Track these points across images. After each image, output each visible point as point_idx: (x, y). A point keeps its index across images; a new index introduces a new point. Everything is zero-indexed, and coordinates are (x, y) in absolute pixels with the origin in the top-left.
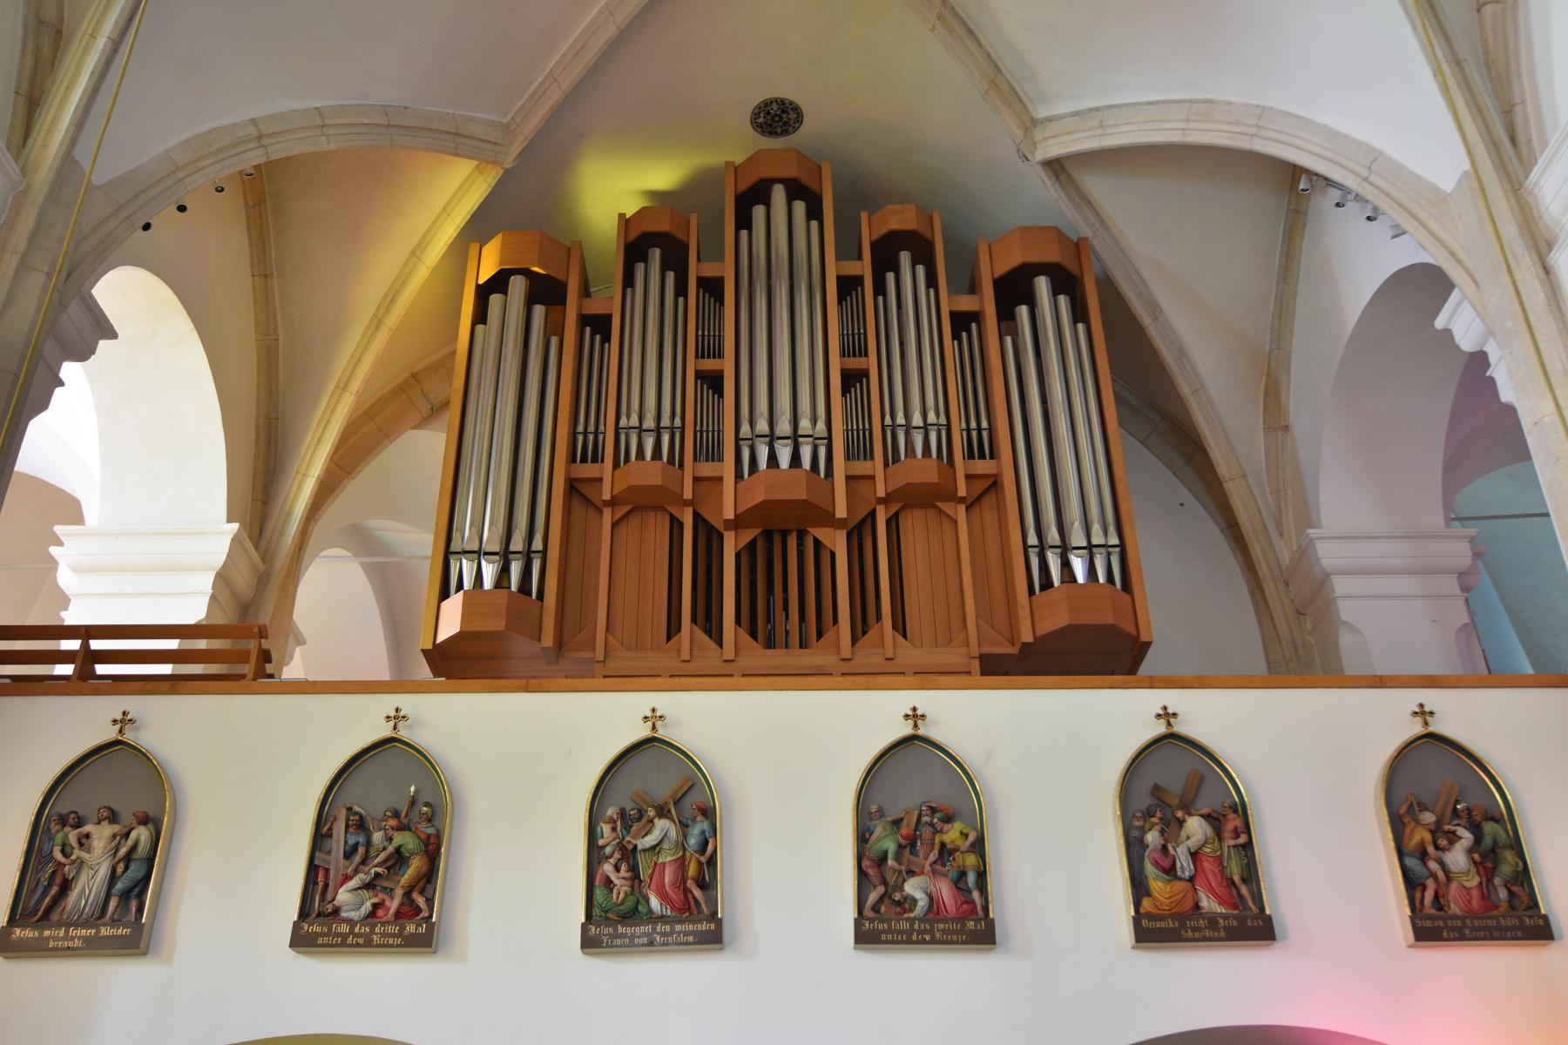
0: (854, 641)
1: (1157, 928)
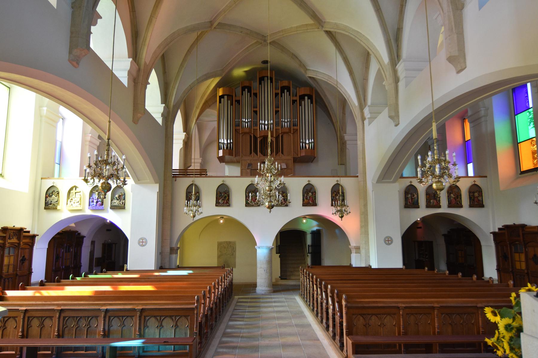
1: (304, 205)
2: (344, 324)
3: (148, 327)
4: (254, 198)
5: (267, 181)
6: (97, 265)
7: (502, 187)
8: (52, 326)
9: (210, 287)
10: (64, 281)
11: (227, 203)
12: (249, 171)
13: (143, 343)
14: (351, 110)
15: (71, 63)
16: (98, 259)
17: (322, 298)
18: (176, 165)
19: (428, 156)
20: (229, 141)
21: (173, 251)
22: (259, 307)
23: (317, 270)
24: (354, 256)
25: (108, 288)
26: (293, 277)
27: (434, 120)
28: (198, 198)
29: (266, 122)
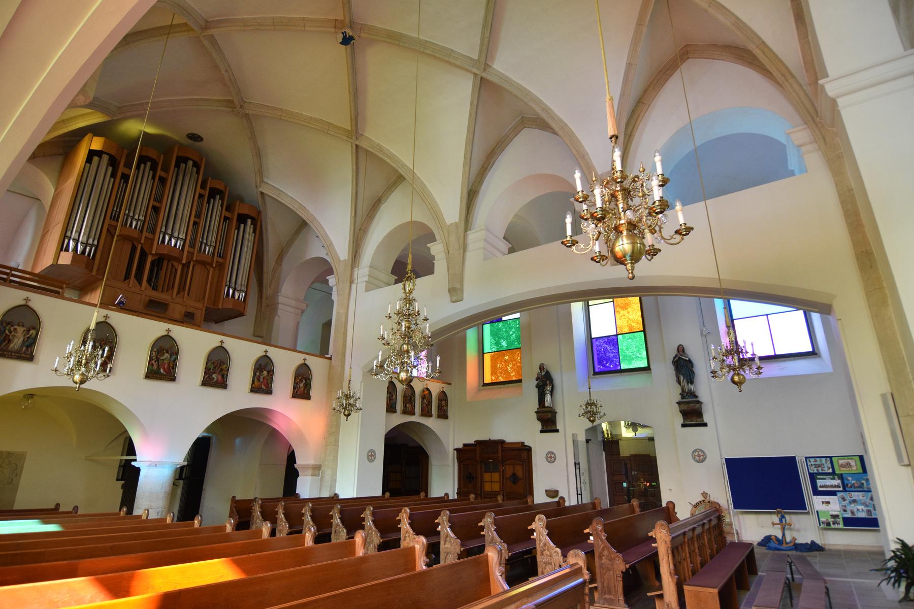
1: (254, 390)
7: (468, 399)
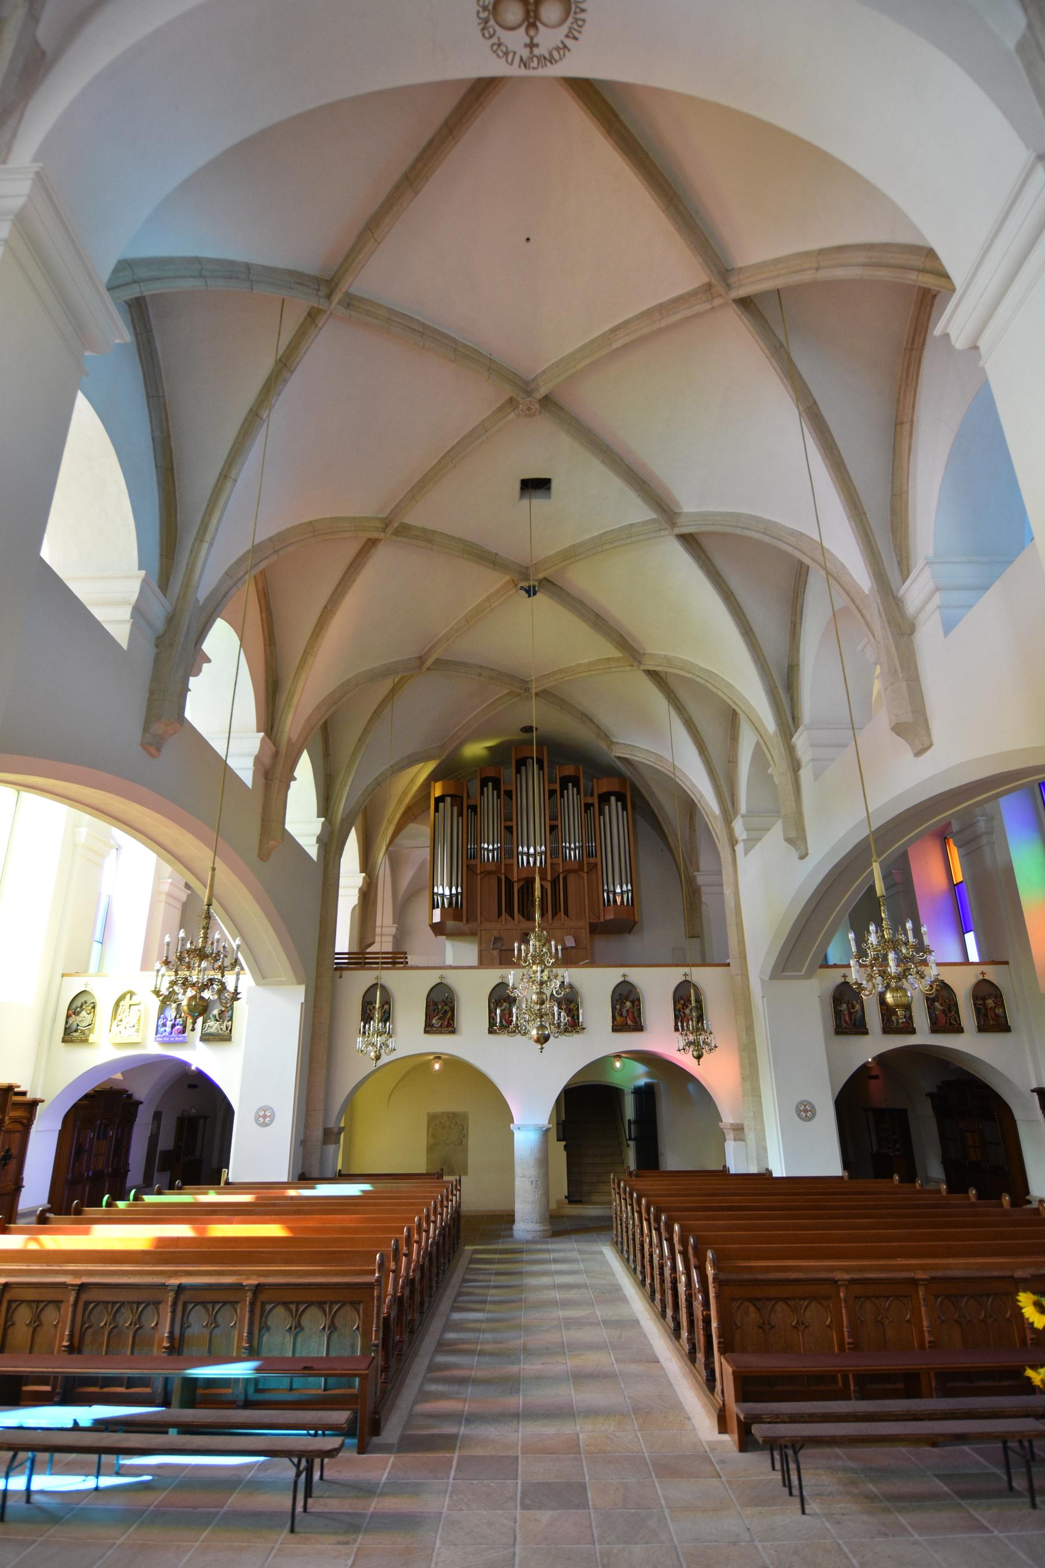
0: (553, 918)
1: (616, 1029)
2: (714, 1325)
3: (268, 1329)
4: (507, 1016)
5: (533, 982)
6: (162, 1169)
8: (59, 1323)
9: (409, 1230)
10: (90, 1211)
11: (449, 1025)
12: (495, 953)
13: (257, 1370)
14: (706, 824)
15: (145, 749)
16: (165, 1154)
17: (661, 1255)
18: (343, 943)
19: (869, 932)
20: (454, 891)
21: (330, 1136)
22: (520, 1273)
23: (649, 1183)
24: (730, 1146)
25: (183, 1231)
26: (595, 1198)
27: (874, 857)
28: (386, 1017)
29: (532, 851)
